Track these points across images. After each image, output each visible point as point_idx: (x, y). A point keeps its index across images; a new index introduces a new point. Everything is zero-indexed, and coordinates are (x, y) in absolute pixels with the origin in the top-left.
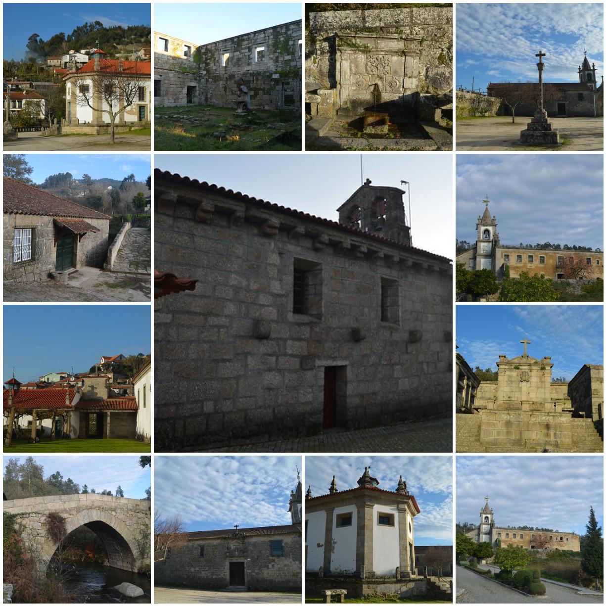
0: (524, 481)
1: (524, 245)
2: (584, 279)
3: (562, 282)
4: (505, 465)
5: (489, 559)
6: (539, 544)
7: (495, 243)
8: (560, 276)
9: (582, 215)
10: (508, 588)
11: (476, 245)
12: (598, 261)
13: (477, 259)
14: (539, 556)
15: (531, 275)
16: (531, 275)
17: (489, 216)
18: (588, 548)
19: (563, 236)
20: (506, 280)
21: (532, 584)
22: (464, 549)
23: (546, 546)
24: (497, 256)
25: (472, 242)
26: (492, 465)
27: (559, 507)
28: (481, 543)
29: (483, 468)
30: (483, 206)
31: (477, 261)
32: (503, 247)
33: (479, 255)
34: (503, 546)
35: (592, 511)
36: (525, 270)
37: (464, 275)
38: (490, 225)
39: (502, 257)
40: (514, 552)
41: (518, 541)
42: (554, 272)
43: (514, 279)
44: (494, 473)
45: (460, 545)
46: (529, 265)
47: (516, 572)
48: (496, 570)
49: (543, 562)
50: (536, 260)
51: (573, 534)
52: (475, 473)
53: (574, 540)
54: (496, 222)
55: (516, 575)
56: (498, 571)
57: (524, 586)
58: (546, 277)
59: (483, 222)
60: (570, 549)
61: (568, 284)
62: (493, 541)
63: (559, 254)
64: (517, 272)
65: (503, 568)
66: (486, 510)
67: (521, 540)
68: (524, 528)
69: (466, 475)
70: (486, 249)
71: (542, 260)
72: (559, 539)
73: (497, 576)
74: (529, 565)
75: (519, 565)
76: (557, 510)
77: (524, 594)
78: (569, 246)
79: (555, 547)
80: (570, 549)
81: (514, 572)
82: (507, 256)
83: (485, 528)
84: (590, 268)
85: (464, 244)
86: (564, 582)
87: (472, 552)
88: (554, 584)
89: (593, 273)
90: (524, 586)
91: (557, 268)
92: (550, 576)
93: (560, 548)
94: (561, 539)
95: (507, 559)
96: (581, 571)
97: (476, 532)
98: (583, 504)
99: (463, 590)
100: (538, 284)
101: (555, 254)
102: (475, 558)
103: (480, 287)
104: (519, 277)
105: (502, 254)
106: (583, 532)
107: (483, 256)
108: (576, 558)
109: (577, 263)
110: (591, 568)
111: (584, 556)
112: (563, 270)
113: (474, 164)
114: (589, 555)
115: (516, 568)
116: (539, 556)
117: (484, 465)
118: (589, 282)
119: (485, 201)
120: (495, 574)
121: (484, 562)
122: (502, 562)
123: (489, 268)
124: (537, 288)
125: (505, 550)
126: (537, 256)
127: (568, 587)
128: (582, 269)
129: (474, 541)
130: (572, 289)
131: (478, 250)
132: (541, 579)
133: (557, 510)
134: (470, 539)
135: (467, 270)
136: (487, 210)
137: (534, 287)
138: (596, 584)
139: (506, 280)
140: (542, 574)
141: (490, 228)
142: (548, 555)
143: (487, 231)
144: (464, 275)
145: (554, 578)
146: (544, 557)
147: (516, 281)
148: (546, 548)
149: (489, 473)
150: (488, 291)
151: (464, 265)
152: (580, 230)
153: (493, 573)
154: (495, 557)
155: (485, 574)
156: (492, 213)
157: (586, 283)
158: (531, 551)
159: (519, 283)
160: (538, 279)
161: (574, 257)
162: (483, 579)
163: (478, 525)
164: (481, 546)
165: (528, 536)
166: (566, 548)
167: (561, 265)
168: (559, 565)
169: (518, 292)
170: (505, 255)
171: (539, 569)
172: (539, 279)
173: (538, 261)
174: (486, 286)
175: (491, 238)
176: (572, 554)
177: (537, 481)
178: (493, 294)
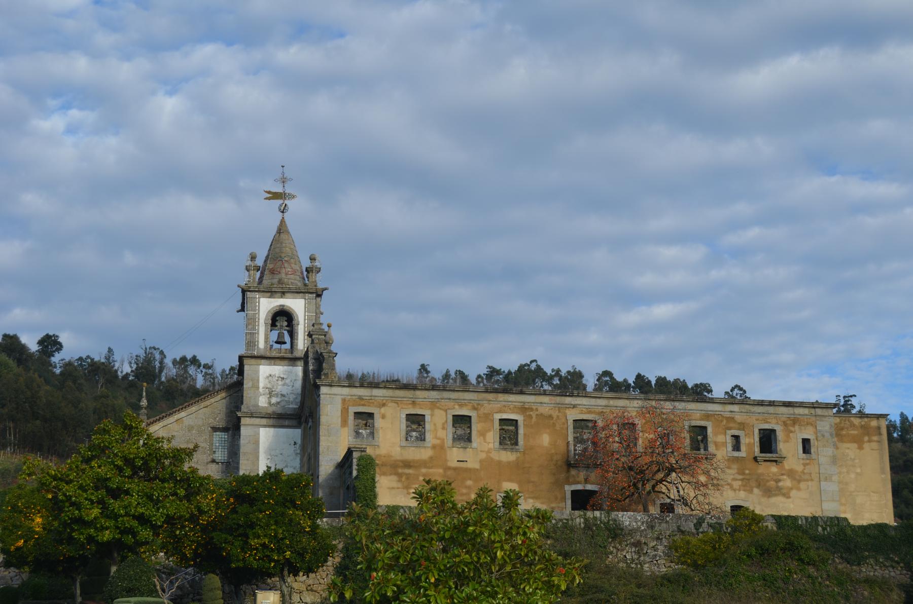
1: (436, 373)
2: (680, 510)
3: (589, 525)
6: (623, 480)
7: (317, 366)
8: (581, 500)
9: (669, 253)
11: (241, 371)
12: (736, 438)
13: (244, 431)
14: (621, 556)
15: (464, 495)
16: (464, 495)
17: (294, 256)
19: (594, 338)
22: (142, 519)
23: (670, 491)
24: (323, 419)
25: (224, 360)
27: (753, 233)
30: (267, 217)
31: (243, 441)
32: (350, 380)
33: (252, 416)
34: (391, 494)
36: (437, 474)
37: (188, 497)
38: (298, 292)
39: (344, 423)
41: (487, 463)
42: (559, 484)
43: (392, 511)
44: (331, 32)
45: (116, 494)
46: (455, 455)
50: (482, 434)
51: (844, 408)
52: (212, 35)
53: (850, 450)
54: (321, 281)
58: (526, 505)
59: (266, 282)
61: (616, 532)
64: (406, 482)
66: (275, 268)
67: (507, 456)
69: (154, 47)
70: (279, 388)
71: (509, 433)
72: (751, 442)
76: (740, 254)
78: (619, 378)
79: (726, 499)
80: (830, 509)
82: (365, 418)
83: (271, 382)
84: (705, 465)
85: (192, 370)
89: (717, 487)
93: (764, 506)
94: (767, 441)
95: (415, 583)
97: (216, 405)
100: (493, 531)
101: (561, 407)
102: (214, 581)
103: (253, 542)
104: (414, 503)
105: (345, 411)
107: (268, 416)
108: (867, 571)
109: (651, 444)
112: (593, 476)
113: (229, 40)
116: (621, 556)
118: (699, 522)
119: (275, 196)
123: (291, 467)
124: (488, 549)
125: (401, 526)
126: (487, 417)
128: (671, 470)
129: (206, 465)
130: (629, 554)
131: (248, 393)
133: (740, 254)
134: (179, 455)
135: (202, 473)
136: (283, 221)
137: (475, 544)
141: (297, 305)
142: (679, 550)
143: (283, 317)
144: (188, 497)
146: (657, 563)
147: (404, 519)
151: (190, 453)
152: (662, 311)
156: (303, 247)
157: (690, 526)
158: (567, 526)
159: (415, 526)
160: (492, 512)
164: (250, 500)
165: (549, 428)
166: (797, 505)
167: (586, 453)
169: (412, 565)
170: (358, 415)
172: (495, 512)
173: (493, 437)
175: (302, 343)
177: (607, 72)
178: (309, 570)
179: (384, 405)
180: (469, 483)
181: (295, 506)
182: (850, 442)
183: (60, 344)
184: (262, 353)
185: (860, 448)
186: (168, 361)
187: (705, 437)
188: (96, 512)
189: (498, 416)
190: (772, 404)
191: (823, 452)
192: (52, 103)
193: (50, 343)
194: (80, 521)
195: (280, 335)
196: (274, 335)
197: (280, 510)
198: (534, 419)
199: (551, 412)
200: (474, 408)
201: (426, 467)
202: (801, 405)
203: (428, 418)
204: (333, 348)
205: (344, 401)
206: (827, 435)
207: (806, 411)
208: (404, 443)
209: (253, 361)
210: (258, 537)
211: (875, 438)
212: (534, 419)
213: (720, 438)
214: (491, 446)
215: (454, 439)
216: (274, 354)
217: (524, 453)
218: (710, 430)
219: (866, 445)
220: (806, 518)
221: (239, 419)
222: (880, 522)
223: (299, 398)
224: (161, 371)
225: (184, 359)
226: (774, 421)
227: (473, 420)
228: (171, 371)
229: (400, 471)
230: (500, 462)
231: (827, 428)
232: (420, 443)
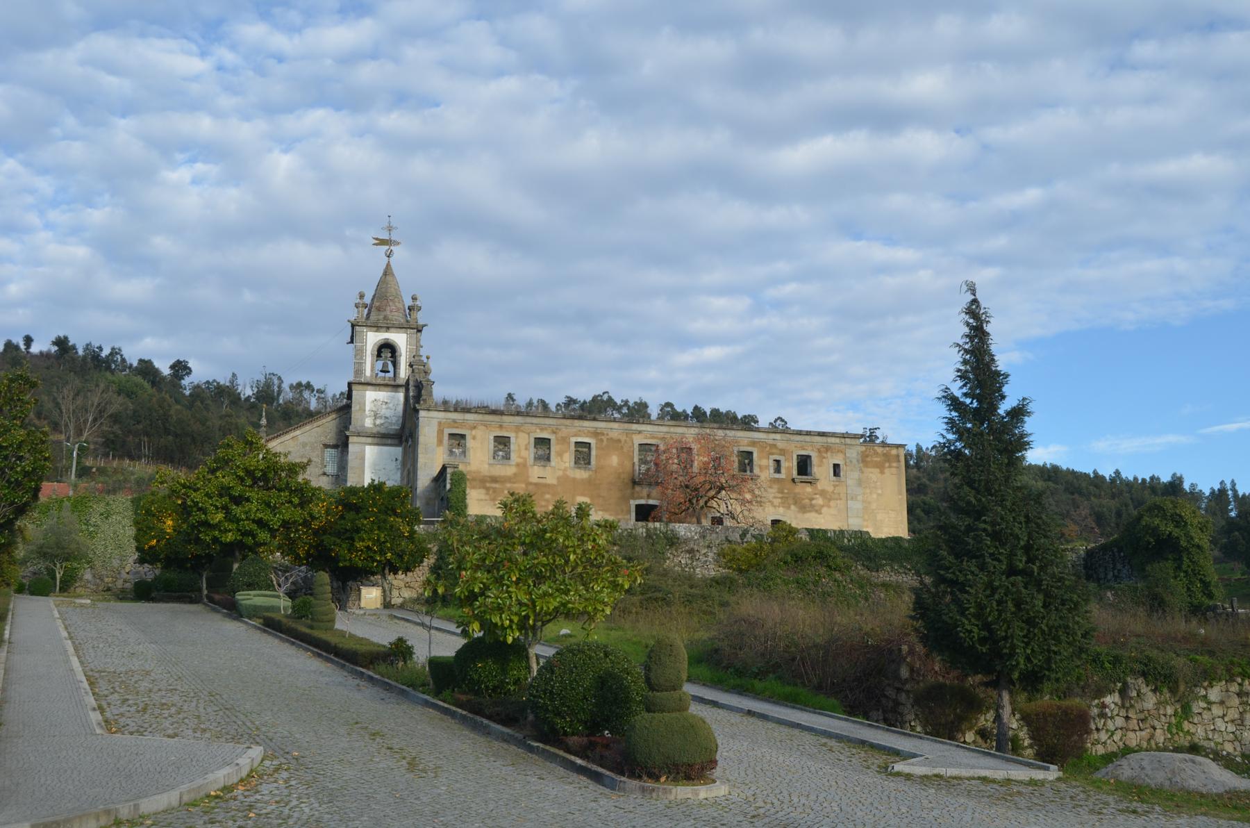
0: (595, 147)
2: (728, 522)
4: (490, 53)
5: (399, 579)
6: (680, 496)
9: (719, 303)
10: (506, 739)
11: (350, 396)
13: (351, 448)
14: (677, 561)
16: (543, 505)
17: (398, 296)
18: (953, 519)
19: (653, 374)
20: (452, 523)
21: (642, 719)
22: (261, 523)
23: (720, 506)
26: (415, 53)
27: (790, 288)
28: (353, 491)
29: (367, 73)
31: (350, 457)
32: (446, 406)
33: (359, 435)
34: (480, 505)
35: (974, 312)
37: (302, 505)
38: (400, 328)
39: (440, 442)
40: (538, 543)
41: (564, 480)
42: (625, 499)
43: (481, 519)
45: (238, 500)
46: (536, 472)
47: (549, 652)
48: (438, 641)
49: (699, 596)
50: (560, 455)
51: (870, 438)
53: (873, 474)
54: (421, 318)
55: (548, 667)
56: (447, 645)
57: (594, 727)
58: (596, 516)
59: (373, 317)
60: (855, 523)
62: (424, 479)
63: (644, 433)
65: (476, 631)
66: (381, 306)
67: (581, 474)
68: (598, 408)
69: (270, 109)
70: (384, 411)
72: (790, 466)
73: (446, 679)
74: (621, 610)
75: (565, 613)
76: (779, 305)
77: (597, 778)
78: (679, 409)
79: (767, 514)
80: (854, 524)
81: (541, 652)
82: (458, 439)
83: (377, 406)
84: (750, 485)
85: (306, 394)
86: (818, 709)
87: (304, 538)
88: (763, 717)
89: (760, 503)
90: (594, 727)
91: (634, 483)
92: (740, 673)
94: (804, 465)
95: (499, 581)
96: (912, 646)
97: (325, 428)
98: (924, 275)
99: (257, 752)
100: (567, 538)
101: (629, 433)
104: (499, 513)
105: (440, 432)
106: (926, 429)
107: (373, 436)
108: (884, 576)
110: (970, 629)
111: (933, 563)
112: (655, 491)
113: (338, 107)
114: (957, 556)
115: (551, 630)
116: (677, 561)
117: (373, 54)
119: (382, 242)
120: (436, 665)
121: (371, 596)
122: (472, 597)
123: (393, 480)
124: (563, 552)
125: (487, 532)
126: (564, 440)
127: (839, 738)
128: (721, 488)
129: (318, 478)
130: (684, 559)
132: (690, 689)
133: (779, 305)
134: (293, 469)
135: (314, 484)
136: (388, 272)
138: (998, 718)
139: (452, 523)
140: (695, 660)
141: (400, 339)
142: (726, 557)
143: (387, 349)
144: (302, 505)
145: (758, 685)
146: (708, 568)
147: (490, 526)
148: (718, 521)
149: (401, 99)
150: (389, 562)
151: (304, 467)
153: (421, 655)
154: (435, 569)
155: (376, 664)
158: (631, 535)
159: (499, 532)
161: (695, 447)
162: (369, 691)
163: (335, 387)
164: (357, 509)
165: (619, 449)
166: (827, 520)
168: (791, 616)
169: (496, 566)
171: (682, 634)
173: (569, 458)
174: (381, 544)
175: (404, 372)
176: (866, 550)
177: (668, 145)
178: (407, 570)
180: (547, 496)
181: (396, 514)
183: (190, 369)
184: (368, 380)
185: (882, 472)
186: (286, 386)
187: (751, 461)
188: (220, 516)
189: (574, 440)
190: (808, 433)
191: (850, 475)
192: (179, 157)
193: (180, 368)
194: (206, 524)
195: (385, 365)
196: (379, 365)
197: (382, 517)
200: (554, 432)
202: (833, 435)
203: (512, 440)
205: (440, 423)
206: (855, 461)
207: (837, 440)
209: (360, 387)
210: (363, 540)
211: (895, 464)
213: (764, 462)
216: (379, 381)
218: (755, 455)
219: (887, 471)
221: (347, 437)
224: (279, 394)
225: (299, 385)
228: (287, 395)
231: (854, 455)
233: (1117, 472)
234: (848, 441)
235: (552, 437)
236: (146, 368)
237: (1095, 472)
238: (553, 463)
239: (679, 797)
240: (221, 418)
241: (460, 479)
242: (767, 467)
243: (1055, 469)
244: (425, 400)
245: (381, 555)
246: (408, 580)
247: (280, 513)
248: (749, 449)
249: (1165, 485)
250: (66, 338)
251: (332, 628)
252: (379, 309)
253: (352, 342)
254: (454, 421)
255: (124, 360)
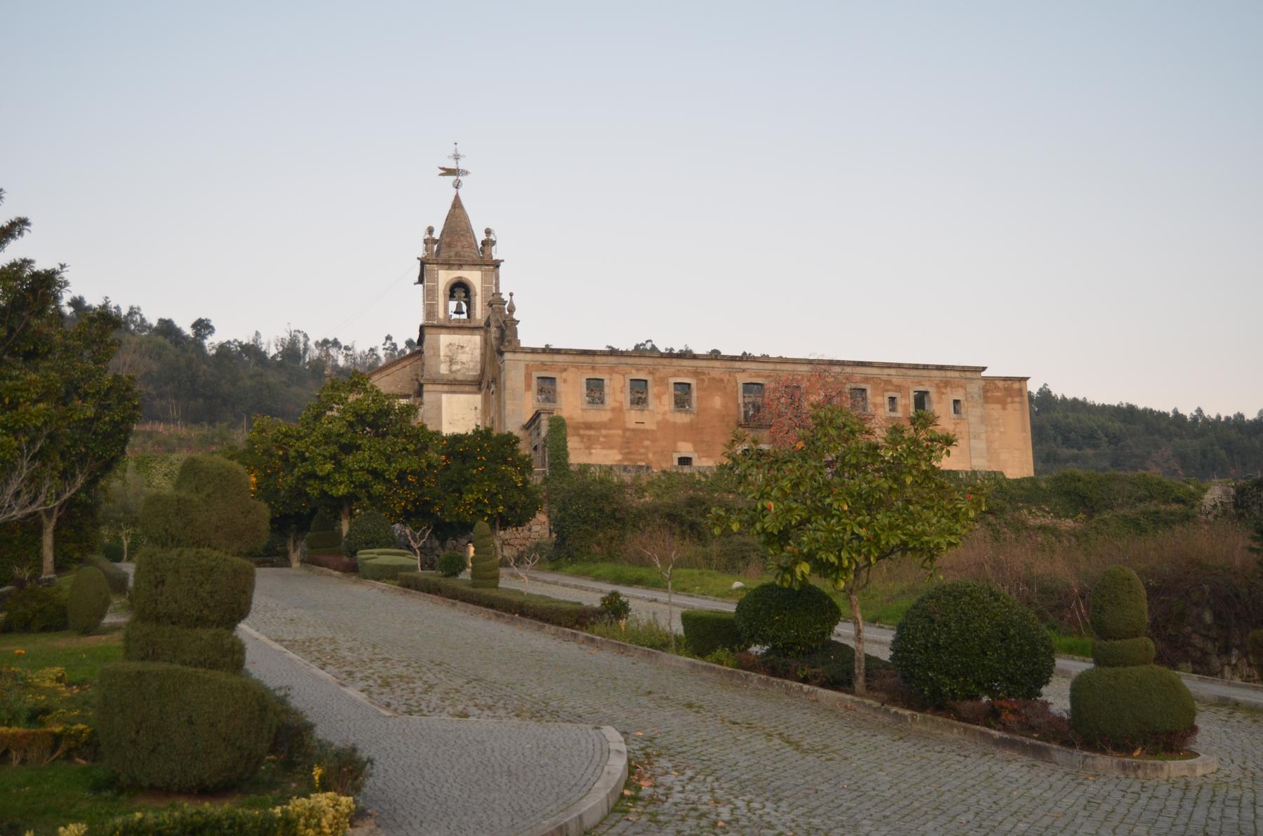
12: (892, 399)
13: (426, 397)
22: (376, 474)
24: (508, 384)
30: (444, 193)
33: (434, 382)
38: (474, 265)
39: (528, 387)
41: (664, 425)
46: (633, 417)
50: (658, 397)
59: (444, 255)
67: (682, 418)
85: (333, 352)
105: (528, 376)
119: (449, 172)
141: (474, 277)
143: (460, 289)
164: (465, 457)
173: (668, 402)
175: (479, 313)
179: (565, 370)
180: (647, 443)
181: (505, 462)
182: (994, 402)
183: (212, 327)
184: (442, 323)
185: (1004, 408)
186: (311, 344)
187: (864, 399)
188: (329, 467)
189: (673, 380)
190: (926, 367)
191: (973, 412)
193: (202, 327)
194: (312, 475)
195: (459, 306)
196: (453, 305)
197: (493, 466)
198: (706, 383)
199: (722, 376)
200: (650, 373)
201: (606, 428)
202: (952, 368)
203: (606, 382)
204: (516, 316)
205: (527, 366)
206: (976, 396)
207: (957, 374)
208: (585, 406)
209: (434, 331)
210: (472, 493)
211: (1017, 399)
212: (706, 383)
213: (879, 400)
214: (667, 408)
215: (632, 403)
216: (453, 324)
217: (698, 414)
218: (869, 392)
219: (1009, 406)
220: (966, 473)
221: (421, 386)
222: (253, 606)
223: (479, 366)
224: (305, 352)
225: (326, 342)
226: (928, 384)
227: (649, 384)
228: (315, 353)
229: (582, 432)
230: (675, 423)
231: (976, 390)
232: (600, 406)
233: (1199, 411)
234: (969, 375)
235: (649, 378)
236: (167, 327)
237: (1175, 411)
238: (651, 407)
239: (1173, 775)
240: (251, 377)
241: (559, 426)
242: (883, 405)
243: (1131, 409)
244: (510, 342)
245: (492, 508)
246: (507, 537)
247: (395, 462)
248: (863, 386)
249: (1250, 422)
250: (81, 299)
251: (496, 587)
252: (449, 245)
253: (421, 280)
254: (543, 364)
255: (143, 320)
